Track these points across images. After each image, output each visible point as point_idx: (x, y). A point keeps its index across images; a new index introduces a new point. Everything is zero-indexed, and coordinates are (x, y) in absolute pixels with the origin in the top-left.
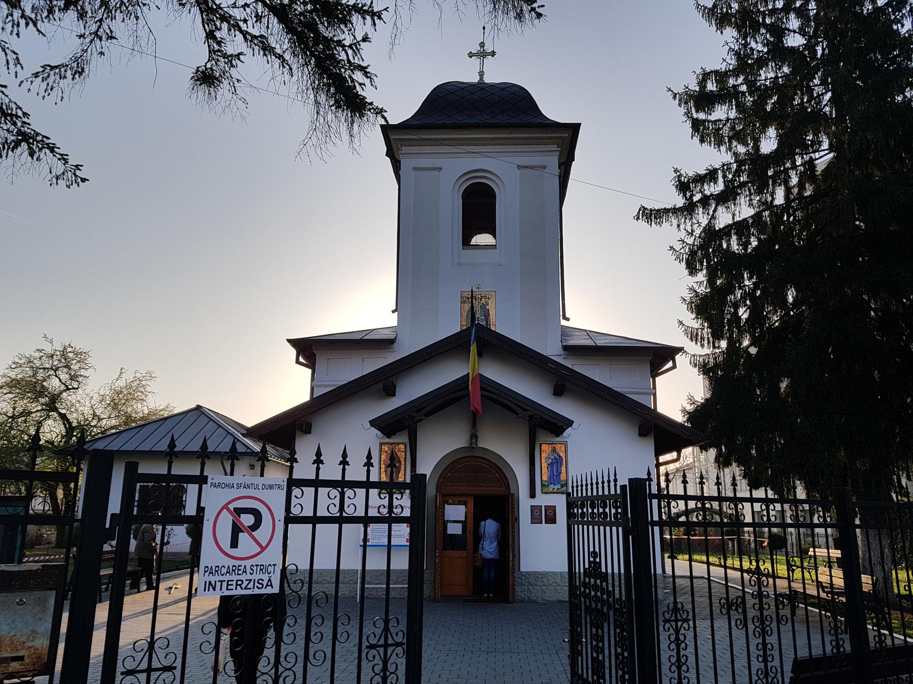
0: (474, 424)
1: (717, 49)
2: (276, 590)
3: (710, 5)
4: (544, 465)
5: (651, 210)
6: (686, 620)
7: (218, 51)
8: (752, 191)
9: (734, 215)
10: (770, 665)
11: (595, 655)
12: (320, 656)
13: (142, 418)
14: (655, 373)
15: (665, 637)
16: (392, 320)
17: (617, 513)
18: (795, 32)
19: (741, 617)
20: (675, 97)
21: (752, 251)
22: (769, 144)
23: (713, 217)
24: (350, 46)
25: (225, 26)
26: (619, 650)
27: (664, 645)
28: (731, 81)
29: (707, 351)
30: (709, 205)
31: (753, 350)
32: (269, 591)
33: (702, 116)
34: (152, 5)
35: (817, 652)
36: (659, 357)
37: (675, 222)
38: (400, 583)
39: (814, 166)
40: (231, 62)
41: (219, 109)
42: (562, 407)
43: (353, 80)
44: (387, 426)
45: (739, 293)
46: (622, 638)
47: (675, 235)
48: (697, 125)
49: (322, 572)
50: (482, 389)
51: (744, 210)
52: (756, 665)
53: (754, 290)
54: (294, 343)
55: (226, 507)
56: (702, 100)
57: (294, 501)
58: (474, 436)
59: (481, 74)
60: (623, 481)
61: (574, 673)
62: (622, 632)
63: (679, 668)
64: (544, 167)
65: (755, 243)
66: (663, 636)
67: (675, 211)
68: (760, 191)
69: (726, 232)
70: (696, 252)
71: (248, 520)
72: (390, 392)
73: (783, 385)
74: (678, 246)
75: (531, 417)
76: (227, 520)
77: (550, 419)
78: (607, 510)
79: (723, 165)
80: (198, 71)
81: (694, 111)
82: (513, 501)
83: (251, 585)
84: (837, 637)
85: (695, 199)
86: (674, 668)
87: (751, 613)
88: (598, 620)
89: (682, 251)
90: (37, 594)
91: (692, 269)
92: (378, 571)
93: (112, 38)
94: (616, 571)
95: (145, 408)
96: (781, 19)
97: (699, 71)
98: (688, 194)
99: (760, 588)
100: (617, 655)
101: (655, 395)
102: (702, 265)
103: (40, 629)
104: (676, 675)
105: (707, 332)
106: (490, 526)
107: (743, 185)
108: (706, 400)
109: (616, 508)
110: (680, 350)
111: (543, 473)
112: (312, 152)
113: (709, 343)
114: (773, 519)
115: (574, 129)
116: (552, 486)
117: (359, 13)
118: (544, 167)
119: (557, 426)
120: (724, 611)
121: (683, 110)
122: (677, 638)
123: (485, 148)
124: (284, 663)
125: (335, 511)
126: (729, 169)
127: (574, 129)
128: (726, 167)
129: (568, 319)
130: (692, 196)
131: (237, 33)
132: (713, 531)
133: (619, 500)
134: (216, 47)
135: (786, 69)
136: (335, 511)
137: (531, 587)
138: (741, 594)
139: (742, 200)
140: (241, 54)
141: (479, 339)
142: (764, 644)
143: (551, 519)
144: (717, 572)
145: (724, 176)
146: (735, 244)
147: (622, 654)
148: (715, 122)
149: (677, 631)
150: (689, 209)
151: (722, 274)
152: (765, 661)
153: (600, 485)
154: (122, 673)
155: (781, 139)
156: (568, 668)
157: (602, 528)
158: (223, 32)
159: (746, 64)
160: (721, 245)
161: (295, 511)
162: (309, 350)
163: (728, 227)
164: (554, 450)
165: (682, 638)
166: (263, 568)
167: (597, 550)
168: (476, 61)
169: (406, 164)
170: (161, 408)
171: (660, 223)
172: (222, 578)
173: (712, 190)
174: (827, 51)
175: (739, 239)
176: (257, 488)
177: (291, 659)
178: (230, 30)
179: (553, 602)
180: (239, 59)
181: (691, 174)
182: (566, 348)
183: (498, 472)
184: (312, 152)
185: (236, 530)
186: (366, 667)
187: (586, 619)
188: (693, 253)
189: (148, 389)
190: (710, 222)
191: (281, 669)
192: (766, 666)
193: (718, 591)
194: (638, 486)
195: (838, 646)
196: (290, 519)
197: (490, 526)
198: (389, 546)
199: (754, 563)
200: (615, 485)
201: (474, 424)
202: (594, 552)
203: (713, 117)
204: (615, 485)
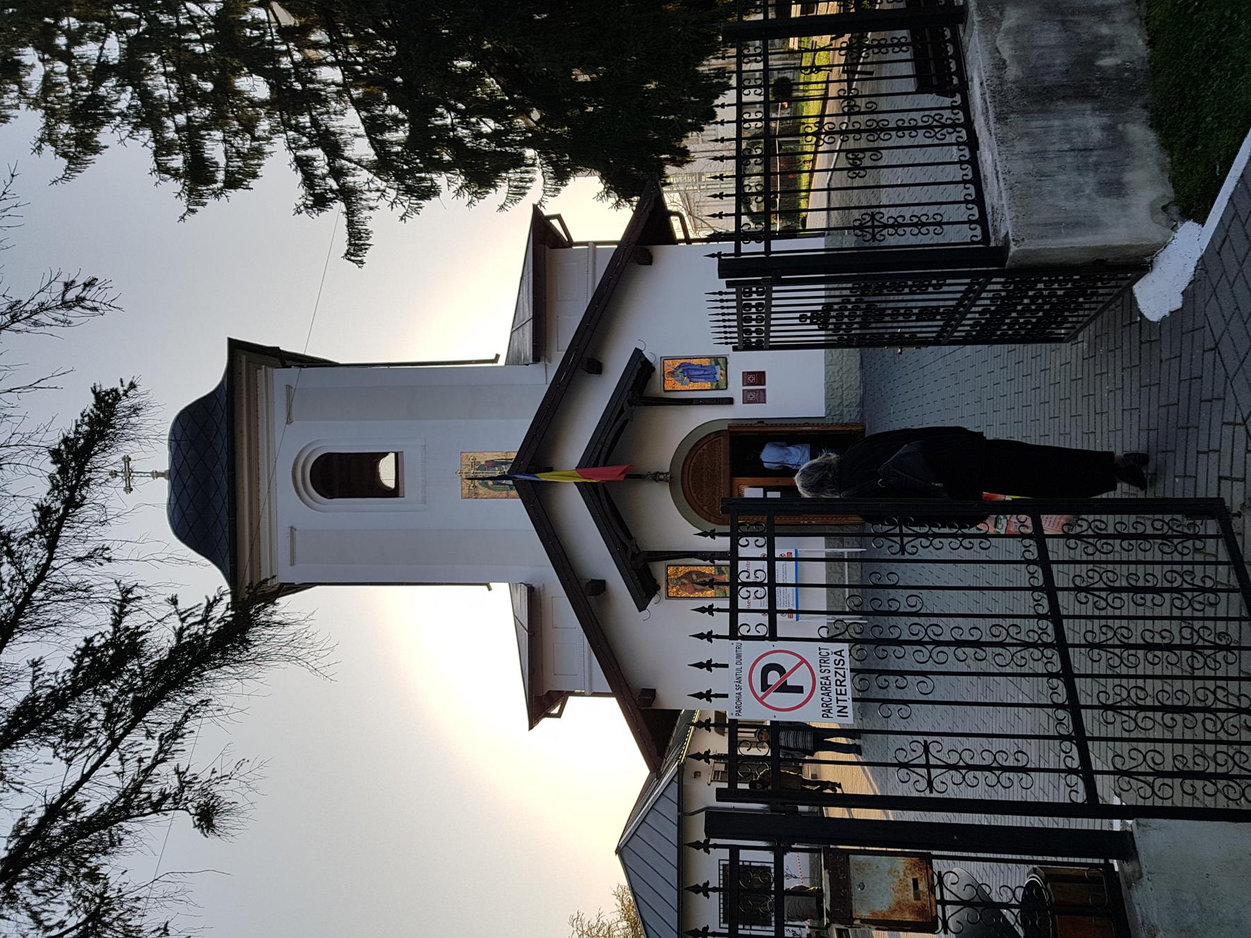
0: (640, 477)
1: (125, 152)
2: (846, 646)
3: (65, 162)
4: (691, 386)
5: (350, 244)
6: (873, 216)
7: (174, 799)
8: (324, 110)
9: (356, 136)
10: (920, 124)
11: (914, 318)
12: (913, 601)
13: (634, 928)
14: (571, 243)
15: (892, 240)
16: (501, 590)
17: (756, 292)
18: (102, 48)
19: (868, 154)
20: (193, 211)
21: (404, 112)
22: (255, 87)
23: (359, 163)
24: (183, 620)
25: (145, 788)
26: (907, 290)
27: (902, 241)
28: (171, 135)
29: (538, 175)
30: (342, 168)
31: (536, 115)
32: (846, 654)
33: (221, 176)
34: (121, 881)
35: (907, 69)
36: (546, 238)
37: (366, 213)
38: (843, 569)
39: (288, 28)
40: (190, 782)
41: (252, 796)
42: (617, 364)
43: (222, 619)
44: (645, 590)
45: (462, 132)
46: (893, 287)
47: (384, 212)
48: (234, 182)
49: (828, 576)
50: (595, 465)
51: (349, 122)
52: (920, 138)
53: (458, 111)
54: (533, 721)
55: (761, 700)
56: (198, 176)
57: (753, 633)
58: (656, 477)
59: (156, 475)
60: (721, 285)
61: (936, 342)
62: (886, 287)
63: (924, 224)
64: (289, 387)
65: (393, 110)
66: (892, 241)
67: (350, 213)
68: (324, 101)
69: (380, 147)
70: (408, 186)
71: (774, 678)
72: (600, 587)
73: (583, 78)
74: (400, 210)
75: (631, 403)
76: (775, 698)
77: (634, 378)
78: (753, 303)
79: (290, 148)
80: (199, 826)
81: (215, 186)
82: (738, 426)
83: (841, 672)
84: (890, 46)
85: (335, 187)
86: (924, 230)
87: (863, 144)
88: (873, 314)
89: (406, 204)
90: (853, 872)
91: (430, 192)
92: (828, 597)
93: (166, 929)
94: (822, 293)
95: (620, 925)
96: (83, 65)
97: (155, 178)
98: (330, 195)
99: (836, 133)
100: (912, 293)
101: (596, 243)
102: (424, 179)
103: (888, 867)
104: (931, 228)
105: (512, 174)
106: (770, 456)
107: (315, 122)
108: (602, 177)
109: (751, 293)
110: (535, 208)
111: (700, 388)
112: (325, 661)
113: (528, 172)
114: (759, 115)
115: (236, 348)
116: (718, 376)
117: (121, 618)
118: (289, 387)
119: (641, 369)
120: (862, 173)
121: (211, 201)
122: (892, 226)
123: (265, 467)
124: (921, 635)
125: (762, 591)
126: (295, 141)
127: (236, 348)
128: (292, 145)
129: (498, 356)
130: (332, 191)
131: (155, 771)
132: (769, 164)
133: (742, 290)
134: (170, 800)
135: (154, 61)
136: (762, 591)
137: (845, 403)
138: (843, 155)
139: (335, 124)
140: (177, 772)
141: (529, 473)
142: (898, 129)
143: (759, 377)
144: (820, 180)
145: (305, 147)
146: (395, 134)
147: (910, 287)
148: (229, 158)
149: (885, 226)
150: (348, 195)
151: (437, 153)
152: (915, 128)
153: (726, 311)
154: (931, 792)
155: (255, 70)
156: (931, 348)
157: (773, 309)
158: (153, 789)
159: (149, 115)
160: (397, 154)
161: (763, 631)
162: (543, 701)
163: (375, 144)
164: (672, 373)
165: (891, 221)
166: (824, 660)
167: (798, 315)
168: (137, 482)
169: (283, 578)
170: (619, 903)
171: (368, 233)
172: (834, 701)
173: (322, 163)
174: (128, 6)
175: (389, 129)
176: (740, 670)
177: (915, 629)
178: (150, 781)
179: (863, 375)
180: (184, 773)
181: (302, 191)
182: (536, 359)
183: (701, 447)
184: (325, 661)
185: (784, 688)
186: (923, 554)
187: (875, 328)
188: (409, 191)
189: (594, 922)
190: (365, 167)
191: (926, 639)
192: (921, 128)
193: (841, 179)
194: (727, 268)
195: (900, 45)
196: (772, 636)
197: (770, 456)
198: (796, 585)
199: (809, 138)
200: (726, 293)
201: (640, 477)
202: (800, 318)
203: (222, 162)
204: (726, 293)
